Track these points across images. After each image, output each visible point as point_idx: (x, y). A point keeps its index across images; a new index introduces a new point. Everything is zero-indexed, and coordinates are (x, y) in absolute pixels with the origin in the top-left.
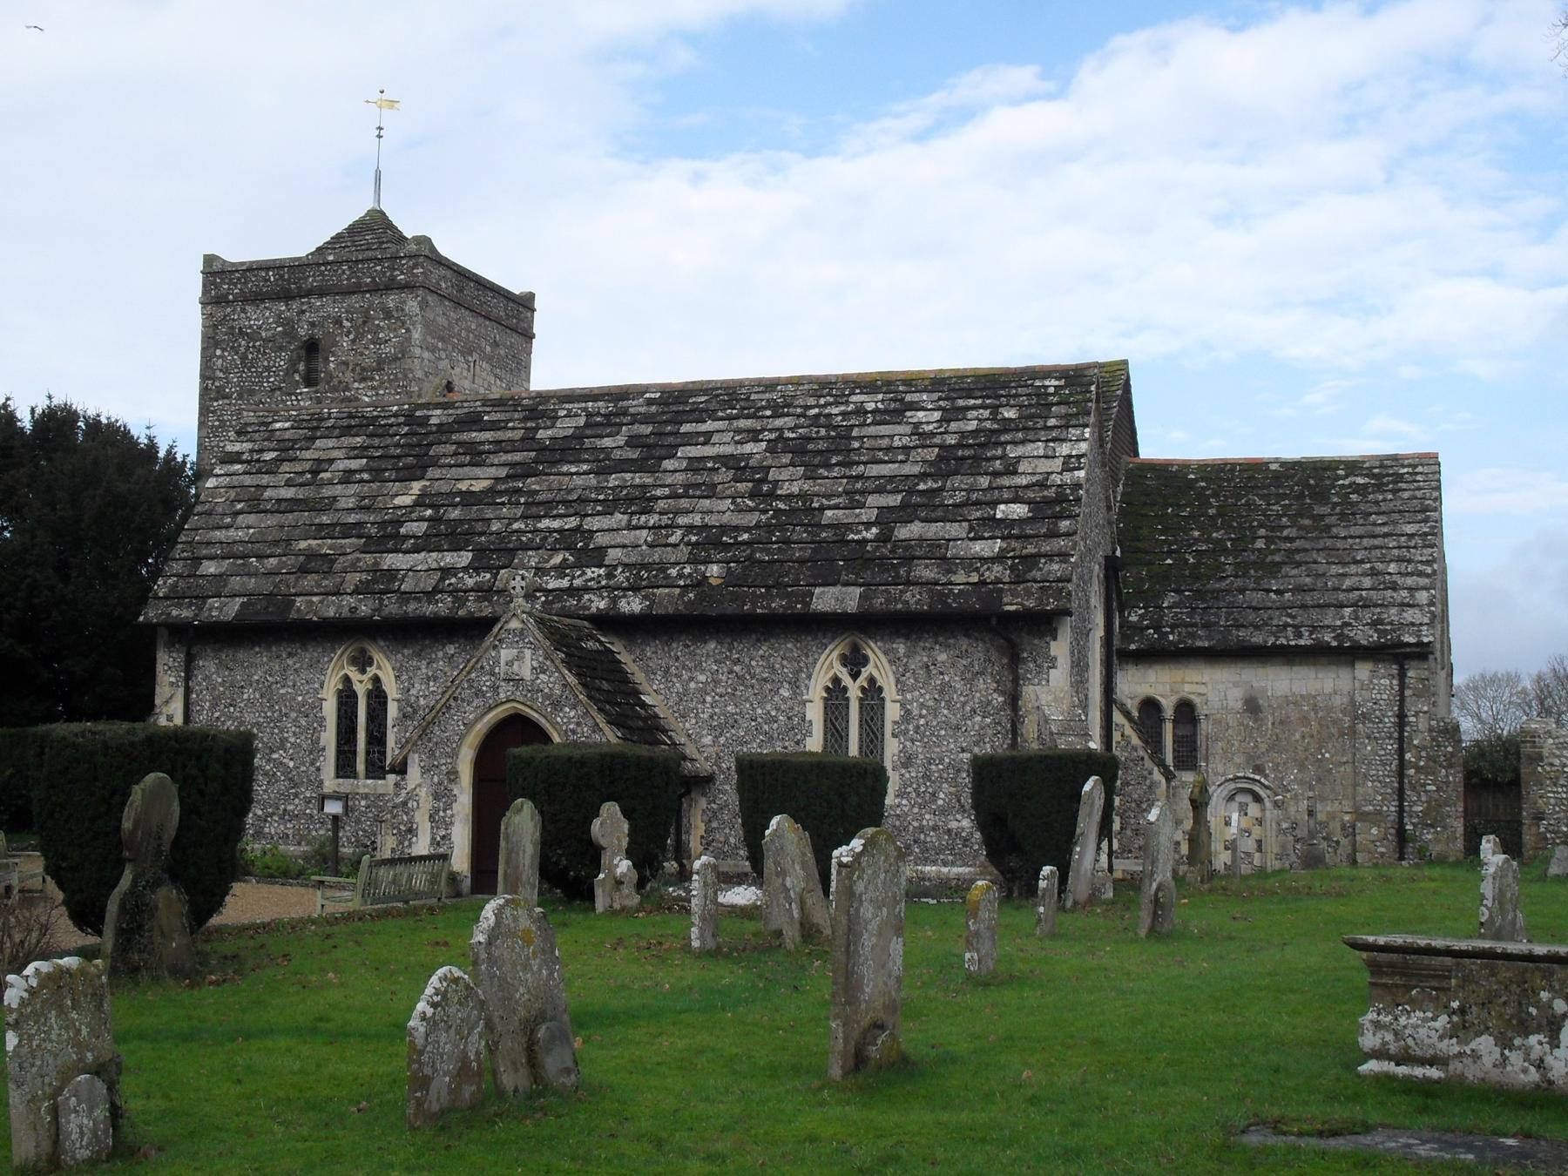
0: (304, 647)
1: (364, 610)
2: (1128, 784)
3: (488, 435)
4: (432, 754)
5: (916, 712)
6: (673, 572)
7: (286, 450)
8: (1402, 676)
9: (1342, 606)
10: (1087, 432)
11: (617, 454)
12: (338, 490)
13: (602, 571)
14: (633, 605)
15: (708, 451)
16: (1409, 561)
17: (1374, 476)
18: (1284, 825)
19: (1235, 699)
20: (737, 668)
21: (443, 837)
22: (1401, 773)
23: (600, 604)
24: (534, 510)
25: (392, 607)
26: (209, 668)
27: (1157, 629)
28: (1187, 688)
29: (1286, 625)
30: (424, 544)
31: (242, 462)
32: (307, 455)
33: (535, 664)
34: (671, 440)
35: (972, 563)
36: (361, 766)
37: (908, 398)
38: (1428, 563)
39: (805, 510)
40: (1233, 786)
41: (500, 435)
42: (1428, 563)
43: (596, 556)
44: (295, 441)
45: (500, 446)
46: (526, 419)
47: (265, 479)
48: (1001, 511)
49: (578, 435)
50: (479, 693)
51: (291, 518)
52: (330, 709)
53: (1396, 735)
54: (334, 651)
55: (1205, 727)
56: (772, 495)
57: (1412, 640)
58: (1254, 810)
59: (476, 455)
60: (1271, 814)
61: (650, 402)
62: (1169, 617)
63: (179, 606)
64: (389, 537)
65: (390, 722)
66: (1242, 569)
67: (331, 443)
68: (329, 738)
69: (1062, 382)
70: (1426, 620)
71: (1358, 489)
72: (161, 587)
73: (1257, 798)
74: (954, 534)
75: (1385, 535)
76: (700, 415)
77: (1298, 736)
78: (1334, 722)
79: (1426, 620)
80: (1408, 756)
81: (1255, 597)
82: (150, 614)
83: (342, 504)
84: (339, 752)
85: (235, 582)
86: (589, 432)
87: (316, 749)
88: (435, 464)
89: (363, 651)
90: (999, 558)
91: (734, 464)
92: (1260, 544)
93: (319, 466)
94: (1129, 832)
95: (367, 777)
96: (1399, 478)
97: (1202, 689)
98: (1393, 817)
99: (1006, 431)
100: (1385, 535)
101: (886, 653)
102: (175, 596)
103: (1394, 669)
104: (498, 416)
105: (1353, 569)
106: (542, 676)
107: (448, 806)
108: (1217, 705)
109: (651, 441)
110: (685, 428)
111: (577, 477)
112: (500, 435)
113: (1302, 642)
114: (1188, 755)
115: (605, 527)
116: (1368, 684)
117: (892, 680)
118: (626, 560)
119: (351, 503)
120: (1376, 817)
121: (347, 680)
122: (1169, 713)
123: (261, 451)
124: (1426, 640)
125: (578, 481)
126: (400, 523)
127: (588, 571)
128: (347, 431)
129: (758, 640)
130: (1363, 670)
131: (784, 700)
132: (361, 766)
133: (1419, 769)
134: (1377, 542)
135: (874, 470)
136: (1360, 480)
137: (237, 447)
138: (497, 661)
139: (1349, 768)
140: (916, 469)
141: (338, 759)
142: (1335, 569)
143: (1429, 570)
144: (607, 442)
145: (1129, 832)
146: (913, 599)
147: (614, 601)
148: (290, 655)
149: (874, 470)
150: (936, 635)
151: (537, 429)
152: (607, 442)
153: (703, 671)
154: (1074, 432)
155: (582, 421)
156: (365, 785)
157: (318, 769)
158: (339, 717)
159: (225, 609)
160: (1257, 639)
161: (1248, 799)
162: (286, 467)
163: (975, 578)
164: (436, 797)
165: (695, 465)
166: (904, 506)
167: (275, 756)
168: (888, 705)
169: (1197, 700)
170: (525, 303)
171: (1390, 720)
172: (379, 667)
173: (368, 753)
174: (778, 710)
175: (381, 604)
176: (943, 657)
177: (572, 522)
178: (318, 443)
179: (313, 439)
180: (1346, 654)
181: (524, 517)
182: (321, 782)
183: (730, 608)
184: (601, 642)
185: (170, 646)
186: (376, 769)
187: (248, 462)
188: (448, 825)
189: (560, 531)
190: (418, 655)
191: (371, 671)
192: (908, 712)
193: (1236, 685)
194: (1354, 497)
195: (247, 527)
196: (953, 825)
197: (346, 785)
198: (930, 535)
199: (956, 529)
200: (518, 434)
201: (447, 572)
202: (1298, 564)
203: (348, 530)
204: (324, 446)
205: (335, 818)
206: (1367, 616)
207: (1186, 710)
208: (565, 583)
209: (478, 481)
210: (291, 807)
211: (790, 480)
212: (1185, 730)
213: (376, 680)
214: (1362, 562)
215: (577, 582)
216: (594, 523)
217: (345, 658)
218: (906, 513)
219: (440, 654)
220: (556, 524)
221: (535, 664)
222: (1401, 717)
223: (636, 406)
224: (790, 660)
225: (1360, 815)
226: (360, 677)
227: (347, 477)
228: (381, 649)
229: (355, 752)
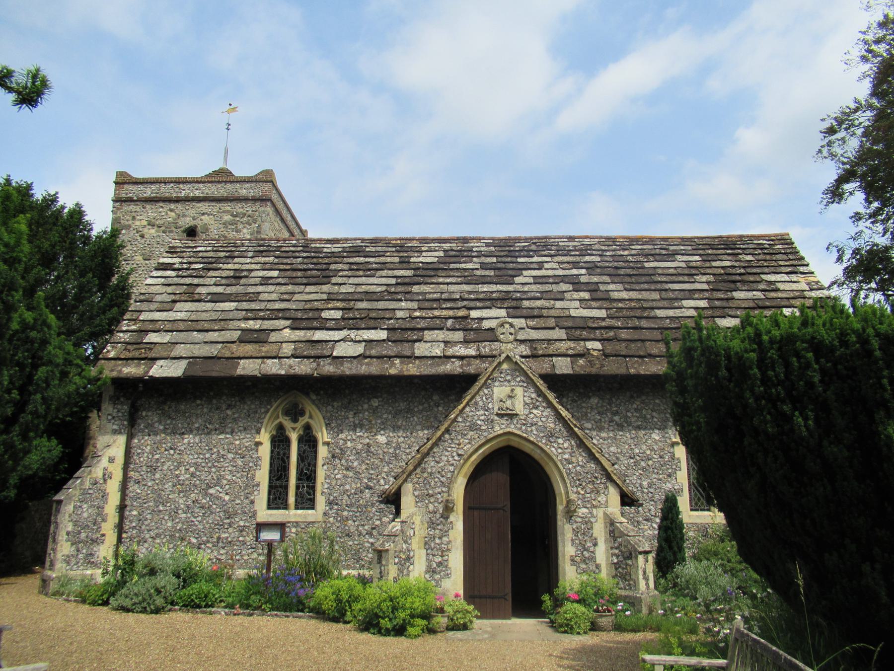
0: (242, 400)
4: (426, 482)
12: (260, 289)
20: (617, 418)
21: (440, 564)
25: (328, 368)
31: (174, 270)
33: (528, 400)
36: (292, 499)
41: (382, 259)
45: (383, 266)
50: (474, 427)
52: (265, 451)
54: (269, 403)
61: (487, 245)
65: (320, 462)
68: (263, 476)
72: (111, 352)
89: (296, 405)
95: (297, 508)
106: (534, 411)
107: (445, 533)
112: (382, 259)
121: (281, 428)
125: (452, 288)
129: (632, 397)
131: (656, 442)
132: (292, 499)
138: (490, 397)
141: (269, 493)
148: (229, 407)
153: (588, 420)
156: (292, 514)
157: (252, 502)
164: (432, 524)
167: (211, 491)
170: (267, 178)
172: (311, 417)
173: (298, 487)
174: (652, 450)
175: (318, 365)
181: (420, 309)
182: (254, 514)
186: (306, 501)
187: (179, 270)
188: (444, 552)
190: (346, 407)
197: (277, 515)
203: (276, 314)
205: (270, 544)
210: (223, 535)
213: (308, 428)
217: (281, 407)
219: (366, 406)
221: (528, 400)
223: (477, 246)
224: (660, 412)
226: (293, 425)
228: (313, 402)
229: (286, 488)
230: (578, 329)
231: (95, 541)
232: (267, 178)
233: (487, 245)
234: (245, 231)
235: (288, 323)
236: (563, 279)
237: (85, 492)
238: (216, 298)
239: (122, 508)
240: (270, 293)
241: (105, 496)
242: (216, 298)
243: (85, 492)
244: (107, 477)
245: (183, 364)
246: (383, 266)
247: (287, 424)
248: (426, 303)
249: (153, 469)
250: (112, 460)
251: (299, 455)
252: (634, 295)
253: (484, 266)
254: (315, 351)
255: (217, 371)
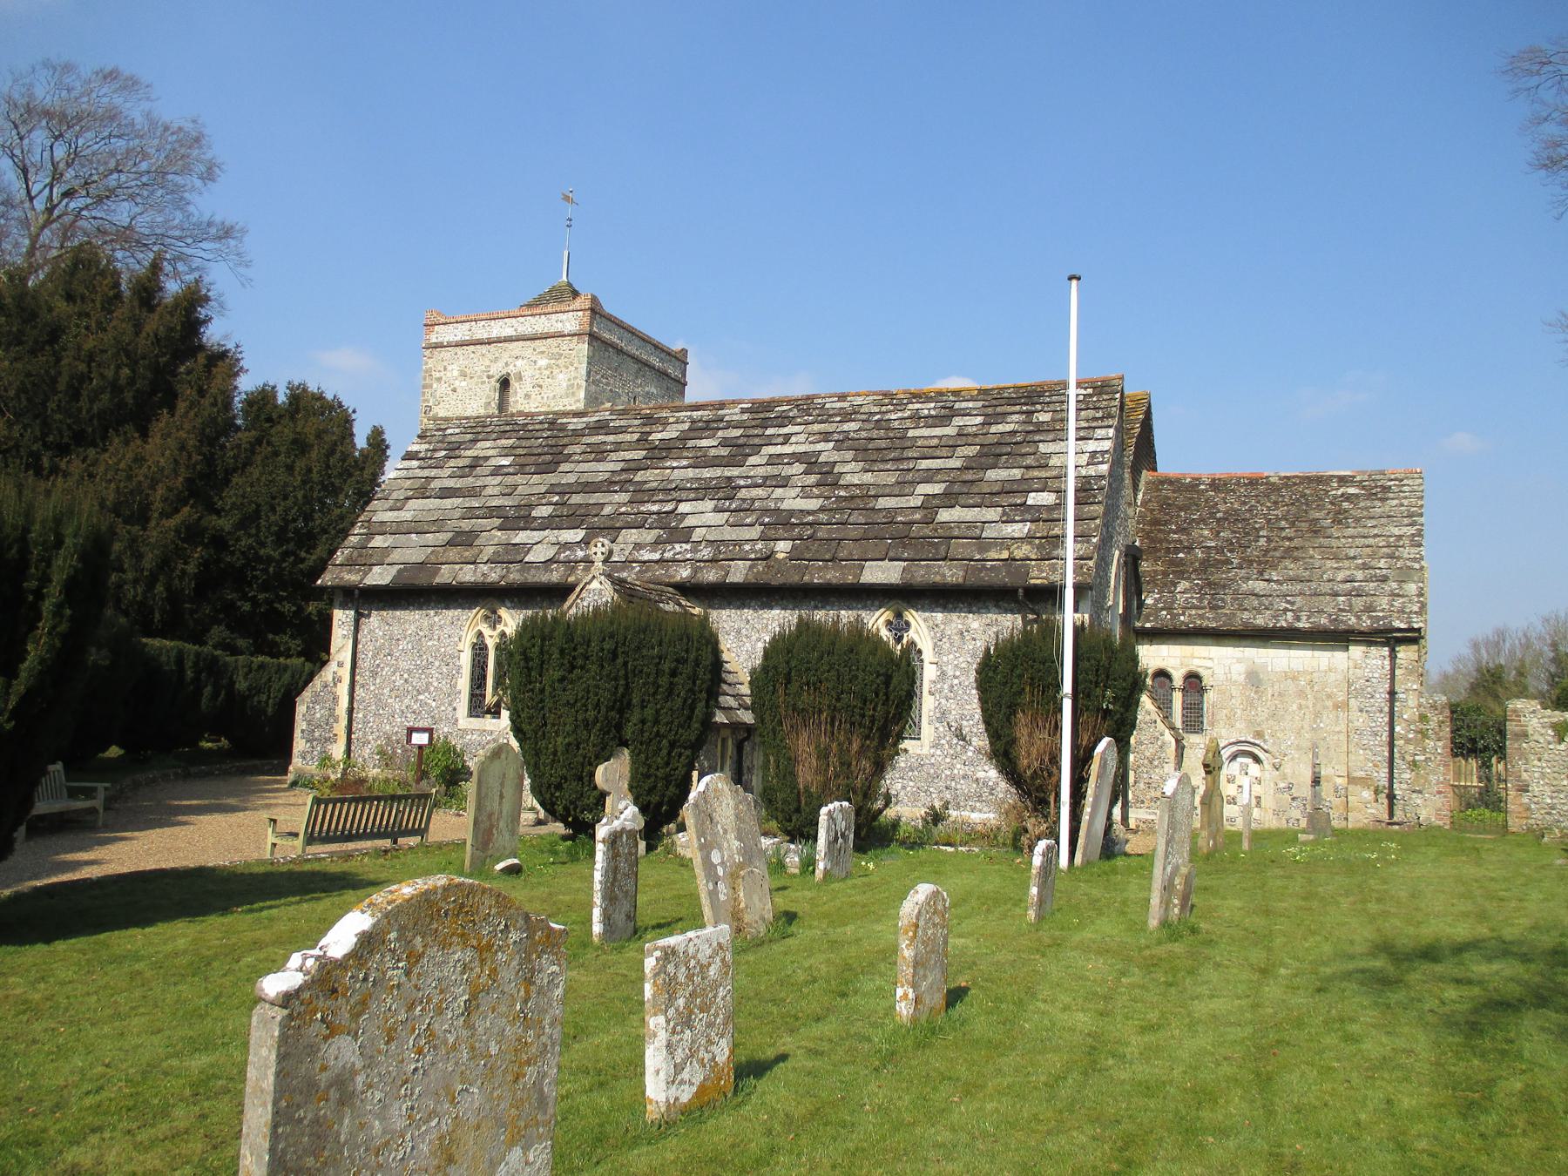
0: (447, 608)
1: (493, 577)
2: (1142, 743)
3: (611, 438)
5: (951, 673)
6: (747, 547)
7: (454, 449)
8: (1393, 657)
9: (1336, 595)
10: (1111, 432)
11: (713, 452)
13: (688, 547)
14: (711, 576)
15: (787, 449)
16: (1398, 558)
17: (1364, 488)
18: (1282, 785)
19: (1239, 673)
22: (1391, 745)
23: (684, 573)
24: (639, 496)
26: (376, 622)
27: (1169, 609)
28: (1197, 662)
29: (1286, 610)
30: (548, 524)
32: (469, 453)
34: (757, 441)
35: (1004, 542)
37: (957, 406)
38: (1415, 560)
39: (862, 498)
40: (1235, 748)
41: (620, 438)
42: (1415, 560)
43: (685, 535)
44: (461, 443)
46: (644, 425)
47: (433, 473)
48: (1032, 499)
49: (683, 438)
51: (448, 503)
52: (466, 660)
53: (1386, 709)
55: (1210, 698)
56: (835, 485)
57: (1403, 626)
58: (1254, 769)
59: (599, 453)
60: (1268, 773)
62: (1181, 599)
63: (350, 572)
64: (519, 519)
66: (1247, 562)
67: (488, 444)
68: (464, 683)
69: (1090, 391)
70: (1416, 609)
71: (1348, 498)
72: (339, 557)
73: (1257, 760)
74: (989, 518)
75: (1376, 536)
76: (784, 420)
77: (1295, 707)
78: (1329, 696)
79: (1416, 609)
80: (1397, 729)
81: (1259, 586)
82: (326, 579)
83: (489, 491)
84: (472, 695)
85: (395, 556)
86: (691, 434)
87: (454, 693)
88: (568, 458)
90: (1029, 538)
91: (810, 461)
92: (1262, 542)
93: (476, 463)
94: (1142, 786)
96: (1386, 489)
97: (1209, 663)
98: (1384, 782)
99: (1038, 431)
100: (1376, 536)
101: (925, 620)
102: (350, 564)
103: (1385, 651)
104: (622, 423)
105: (1347, 563)
108: (1222, 677)
109: (741, 441)
110: (769, 431)
111: (680, 471)
112: (620, 438)
113: (1301, 625)
114: (1194, 720)
115: (702, 516)
116: (1366, 661)
117: (931, 645)
118: (709, 537)
119: (496, 491)
120: (1364, 782)
121: (480, 634)
122: (1178, 681)
123: (434, 450)
124: (1416, 626)
126: (531, 506)
127: (677, 546)
128: (503, 434)
130: (1356, 651)
133: (1408, 741)
134: (1371, 541)
135: (924, 464)
136: (1352, 490)
137: (415, 448)
139: (1343, 737)
140: (957, 463)
141: (471, 701)
142: (1329, 564)
143: (1417, 566)
144: (704, 443)
145: (1142, 786)
146: (951, 574)
147: (695, 571)
149: (924, 464)
150: (970, 605)
151: (650, 433)
152: (704, 443)
154: (1100, 433)
155: (686, 426)
158: (473, 666)
159: (380, 576)
160: (1260, 621)
161: (1249, 761)
162: (452, 463)
163: (1005, 555)
165: (774, 460)
166: (945, 494)
168: (926, 665)
169: (1202, 672)
171: (1381, 697)
176: (975, 625)
177: (669, 507)
178: (479, 445)
179: (475, 441)
180: (1338, 637)
183: (795, 579)
184: (680, 605)
185: (344, 607)
189: (658, 513)
191: (500, 628)
192: (943, 673)
193: (1239, 661)
194: (1345, 505)
195: (414, 509)
196: (981, 775)
198: (968, 518)
199: (992, 514)
200: (636, 436)
201: (566, 546)
202: (1296, 559)
203: (492, 512)
204: (483, 448)
205: (421, 747)
206: (1359, 603)
207: (1194, 681)
208: (656, 556)
209: (602, 470)
211: (853, 474)
212: (1192, 698)
214: (1354, 558)
215: (668, 555)
216: (684, 508)
218: (950, 499)
220: (655, 508)
222: (1392, 693)
223: (733, 414)
225: (1352, 780)
227: (497, 471)
230: (782, 522)
231: (327, 740)
232: (681, 359)
233: (743, 411)
234: (561, 376)
235: (497, 522)
236: (797, 457)
237: (317, 695)
238: (446, 493)
239: (351, 711)
240: (493, 484)
241: (335, 699)
242: (446, 493)
243: (317, 695)
244: (337, 680)
245: (394, 570)
246: (618, 447)
247: (487, 632)
248: (642, 494)
249: (374, 674)
250: (340, 665)
251: (1061, 710)
252: (54, 593)
253: (725, 443)
254: (512, 555)
255: (422, 580)
